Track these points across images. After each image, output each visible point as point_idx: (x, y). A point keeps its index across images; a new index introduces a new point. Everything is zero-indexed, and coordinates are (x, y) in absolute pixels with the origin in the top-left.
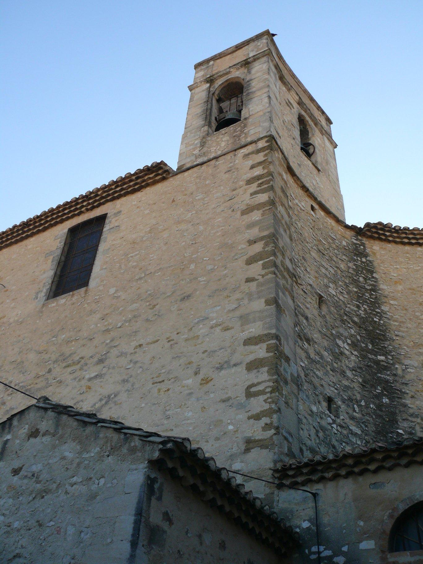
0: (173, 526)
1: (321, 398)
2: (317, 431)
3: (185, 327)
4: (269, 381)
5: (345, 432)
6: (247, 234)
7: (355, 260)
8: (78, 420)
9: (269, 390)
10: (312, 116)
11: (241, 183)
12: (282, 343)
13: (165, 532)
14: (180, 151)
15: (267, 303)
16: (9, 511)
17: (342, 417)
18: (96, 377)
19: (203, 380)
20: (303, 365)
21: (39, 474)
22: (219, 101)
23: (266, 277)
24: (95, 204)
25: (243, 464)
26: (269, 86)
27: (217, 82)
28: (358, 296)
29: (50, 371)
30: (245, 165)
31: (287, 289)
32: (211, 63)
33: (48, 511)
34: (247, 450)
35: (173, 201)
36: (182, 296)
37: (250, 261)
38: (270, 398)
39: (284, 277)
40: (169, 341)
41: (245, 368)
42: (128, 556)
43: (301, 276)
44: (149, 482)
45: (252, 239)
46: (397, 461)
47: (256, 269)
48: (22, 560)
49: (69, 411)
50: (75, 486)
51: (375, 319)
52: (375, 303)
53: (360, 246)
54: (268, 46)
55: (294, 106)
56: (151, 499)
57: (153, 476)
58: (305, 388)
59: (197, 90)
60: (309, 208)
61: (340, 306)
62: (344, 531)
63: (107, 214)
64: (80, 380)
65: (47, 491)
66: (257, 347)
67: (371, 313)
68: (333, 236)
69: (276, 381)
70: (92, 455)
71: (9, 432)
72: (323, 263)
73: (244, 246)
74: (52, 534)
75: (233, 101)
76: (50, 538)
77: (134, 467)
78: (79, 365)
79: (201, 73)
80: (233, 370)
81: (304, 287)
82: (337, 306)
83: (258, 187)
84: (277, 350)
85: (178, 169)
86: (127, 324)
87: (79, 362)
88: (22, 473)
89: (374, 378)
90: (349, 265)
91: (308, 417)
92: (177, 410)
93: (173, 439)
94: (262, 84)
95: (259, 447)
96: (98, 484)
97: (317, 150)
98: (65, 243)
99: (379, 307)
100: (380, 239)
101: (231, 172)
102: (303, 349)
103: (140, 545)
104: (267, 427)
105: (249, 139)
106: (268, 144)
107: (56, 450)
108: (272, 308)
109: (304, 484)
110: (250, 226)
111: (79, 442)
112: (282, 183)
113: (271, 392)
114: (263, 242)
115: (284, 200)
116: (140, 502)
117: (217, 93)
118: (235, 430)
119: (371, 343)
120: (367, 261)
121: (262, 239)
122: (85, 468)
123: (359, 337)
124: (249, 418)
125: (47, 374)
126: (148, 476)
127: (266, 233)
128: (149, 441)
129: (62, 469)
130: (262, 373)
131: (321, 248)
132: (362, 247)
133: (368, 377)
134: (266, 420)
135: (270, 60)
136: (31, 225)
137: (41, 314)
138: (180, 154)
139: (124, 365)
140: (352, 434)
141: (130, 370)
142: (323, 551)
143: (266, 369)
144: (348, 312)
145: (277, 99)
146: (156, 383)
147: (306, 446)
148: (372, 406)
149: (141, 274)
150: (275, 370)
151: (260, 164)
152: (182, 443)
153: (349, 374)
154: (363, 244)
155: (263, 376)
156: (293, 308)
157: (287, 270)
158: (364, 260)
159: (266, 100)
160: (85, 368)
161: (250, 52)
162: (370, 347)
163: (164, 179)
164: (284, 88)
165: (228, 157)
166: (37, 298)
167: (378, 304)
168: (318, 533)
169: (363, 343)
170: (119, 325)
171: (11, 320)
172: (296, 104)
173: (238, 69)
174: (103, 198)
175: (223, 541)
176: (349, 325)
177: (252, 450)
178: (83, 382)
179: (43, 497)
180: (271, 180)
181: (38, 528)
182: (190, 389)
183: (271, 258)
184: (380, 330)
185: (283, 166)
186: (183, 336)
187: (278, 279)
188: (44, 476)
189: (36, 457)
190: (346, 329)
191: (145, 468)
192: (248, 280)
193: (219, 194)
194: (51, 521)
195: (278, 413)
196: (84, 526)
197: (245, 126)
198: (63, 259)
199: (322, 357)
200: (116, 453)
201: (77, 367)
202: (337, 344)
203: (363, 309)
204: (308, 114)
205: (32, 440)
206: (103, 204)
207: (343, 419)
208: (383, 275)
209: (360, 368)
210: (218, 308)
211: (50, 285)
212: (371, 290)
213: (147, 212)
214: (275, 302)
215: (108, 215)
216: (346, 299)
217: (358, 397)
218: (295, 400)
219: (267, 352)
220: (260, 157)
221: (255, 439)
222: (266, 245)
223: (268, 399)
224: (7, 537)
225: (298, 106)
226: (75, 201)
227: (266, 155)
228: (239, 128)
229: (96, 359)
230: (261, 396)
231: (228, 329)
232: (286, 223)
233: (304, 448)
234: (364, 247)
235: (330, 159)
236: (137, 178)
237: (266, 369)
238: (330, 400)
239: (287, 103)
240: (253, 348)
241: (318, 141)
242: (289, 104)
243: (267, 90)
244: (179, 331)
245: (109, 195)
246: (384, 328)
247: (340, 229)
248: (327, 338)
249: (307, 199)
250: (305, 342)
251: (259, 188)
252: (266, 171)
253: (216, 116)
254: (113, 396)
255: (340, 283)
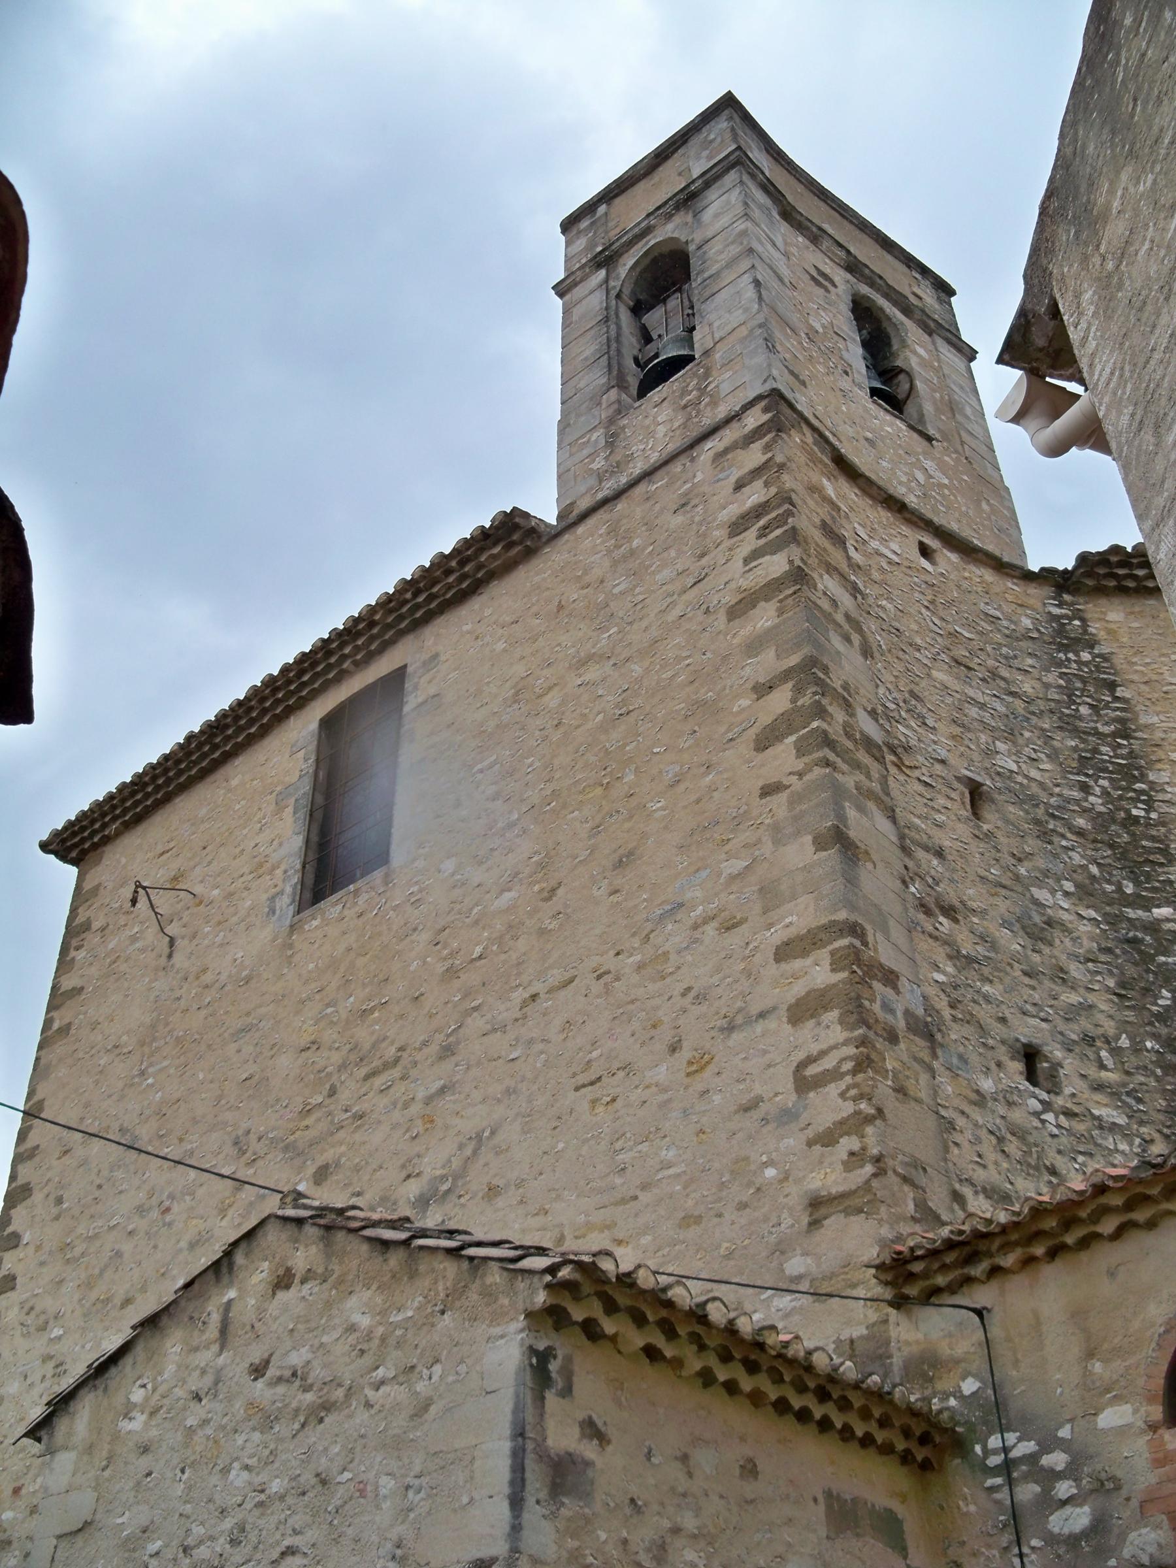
0: (610, 1448)
1: (1002, 1053)
2: (1001, 1140)
3: (634, 935)
4: (846, 1043)
5: (1080, 1127)
6: (748, 669)
7: (1060, 664)
8: (369, 1239)
9: (848, 1066)
10: (891, 294)
11: (717, 533)
12: (870, 939)
13: (588, 1464)
14: (559, 465)
15: (820, 844)
16: (255, 1459)
17: (1068, 1091)
18: (442, 1091)
19: (690, 1063)
20: (941, 978)
21: (306, 1370)
22: (638, 309)
23: (807, 778)
24: (373, 647)
25: (809, 1261)
26: (751, 250)
27: (621, 261)
28: (1081, 757)
29: (332, 1092)
30: (719, 487)
31: (870, 795)
32: (602, 209)
33: (337, 1450)
34: (815, 1224)
35: (560, 607)
36: (616, 857)
37: (764, 742)
38: (855, 1085)
39: (857, 766)
40: (599, 978)
41: (785, 1019)
42: (507, 1529)
43: (913, 742)
44: (534, 1361)
45: (762, 680)
46: (1092, 1228)
47: (783, 758)
48: (298, 1560)
49: (349, 1218)
50: (383, 1389)
51: (1135, 812)
52: (1131, 772)
53: (1071, 619)
54: (735, 136)
55: (837, 279)
56: (543, 1398)
57: (541, 1346)
58: (954, 1037)
59: (578, 292)
60: (915, 553)
61: (1032, 797)
62: (1059, 1390)
63: (405, 666)
64: (406, 1106)
65: (327, 1407)
66: (809, 961)
67: (1121, 798)
68: (992, 612)
69: (863, 1042)
70: (410, 1314)
71: (230, 1284)
72: (971, 692)
73: (745, 702)
74: (351, 1498)
75: (674, 302)
76: (347, 1507)
77: (497, 1331)
78: (399, 1068)
79: (581, 243)
80: (759, 1028)
81: (924, 770)
82: (1025, 799)
83: (759, 537)
84: (858, 960)
85: (560, 517)
86: (495, 948)
87: (397, 1061)
88: (271, 1372)
89: (1148, 971)
90: (1045, 679)
91: (968, 1109)
92: (640, 1147)
93: (572, 1257)
94: (735, 250)
95: (840, 1212)
96: (430, 1378)
97: (919, 384)
98: (317, 761)
99: (1143, 778)
100: (1122, 590)
101: (688, 508)
102: (936, 939)
103: (530, 1501)
104: (855, 1158)
105: (722, 412)
106: (769, 415)
107: (335, 1312)
108: (832, 855)
109: (952, 1289)
110: (753, 647)
111: (379, 1288)
112: (824, 512)
113: (854, 1072)
114: (790, 685)
115: (836, 556)
116: (518, 1409)
117: (627, 291)
118: (781, 1176)
119: (1130, 879)
120: (1095, 656)
121: (786, 675)
122: (398, 1345)
123: (1094, 870)
124: (810, 1144)
125: (328, 1101)
126: (531, 1348)
127: (794, 660)
128: (523, 1271)
129: (353, 1354)
130: (828, 1027)
131: (961, 652)
132: (1077, 622)
133: (1131, 971)
134: (849, 1143)
135: (746, 178)
136: (227, 726)
137: (289, 953)
138: (559, 477)
139: (503, 1053)
140: (1101, 1128)
141: (517, 1063)
142: (1014, 1446)
143: (834, 1015)
144: (1059, 808)
145: (781, 279)
146: (584, 1086)
147: (973, 1185)
148: (1149, 1044)
149: (510, 812)
150: (857, 1013)
151: (756, 472)
152: (594, 1263)
153: (1076, 971)
154: (1078, 615)
155: (830, 1035)
156: (894, 839)
157: (868, 743)
158: (1086, 656)
159: (750, 293)
160: (414, 1073)
161: (697, 163)
162: (1129, 889)
163: (529, 553)
164: (800, 239)
165: (677, 467)
166: (274, 913)
167: (1137, 769)
168: (999, 1406)
169: (1109, 882)
170: (478, 950)
171: (223, 977)
172: (842, 272)
173: (669, 217)
174: (389, 627)
175: (750, 1460)
176: (1064, 843)
177: (826, 1223)
178: (415, 1109)
179: (321, 1420)
180: (789, 513)
181: (319, 1488)
182: (665, 1090)
183: (815, 724)
184: (1153, 839)
185: (821, 461)
186: (631, 959)
187: (839, 776)
188: (318, 1373)
189: (295, 1334)
190: (1056, 856)
191: (522, 1331)
192: (767, 791)
193: (666, 574)
194: (344, 1469)
195: (878, 1122)
196: (412, 1474)
197: (707, 374)
198: (320, 800)
199: (994, 946)
200: (458, 1304)
201: (396, 1073)
202: (1036, 902)
203: (1098, 790)
204: (878, 290)
205: (282, 1295)
206: (392, 642)
207: (1073, 1095)
208: (1143, 687)
209: (1108, 951)
210: (704, 874)
211: (300, 875)
212: (1114, 735)
213: (501, 646)
214: (838, 838)
215: (410, 670)
216: (1047, 775)
217: (1109, 1027)
218: (924, 1077)
219: (833, 970)
220: (755, 456)
221: (829, 1194)
222: (798, 691)
223: (848, 1089)
224: (262, 1514)
225: (849, 276)
226: (322, 648)
227: (767, 448)
228: (695, 382)
229: (434, 1048)
230: (833, 1085)
231: (734, 926)
232: (847, 616)
233: (967, 1191)
234: (1083, 620)
235: (959, 395)
236: (462, 563)
237: (834, 1015)
238: (1030, 1056)
239: (813, 278)
240: (798, 964)
241: (919, 356)
242: (821, 280)
243: (745, 264)
244: (619, 948)
245: (401, 618)
246: (1163, 830)
247: (1013, 586)
248: (1003, 892)
249: (905, 529)
250: (941, 919)
251: (763, 541)
252: (773, 490)
253: (635, 352)
254: (486, 1134)
255: (1027, 734)
